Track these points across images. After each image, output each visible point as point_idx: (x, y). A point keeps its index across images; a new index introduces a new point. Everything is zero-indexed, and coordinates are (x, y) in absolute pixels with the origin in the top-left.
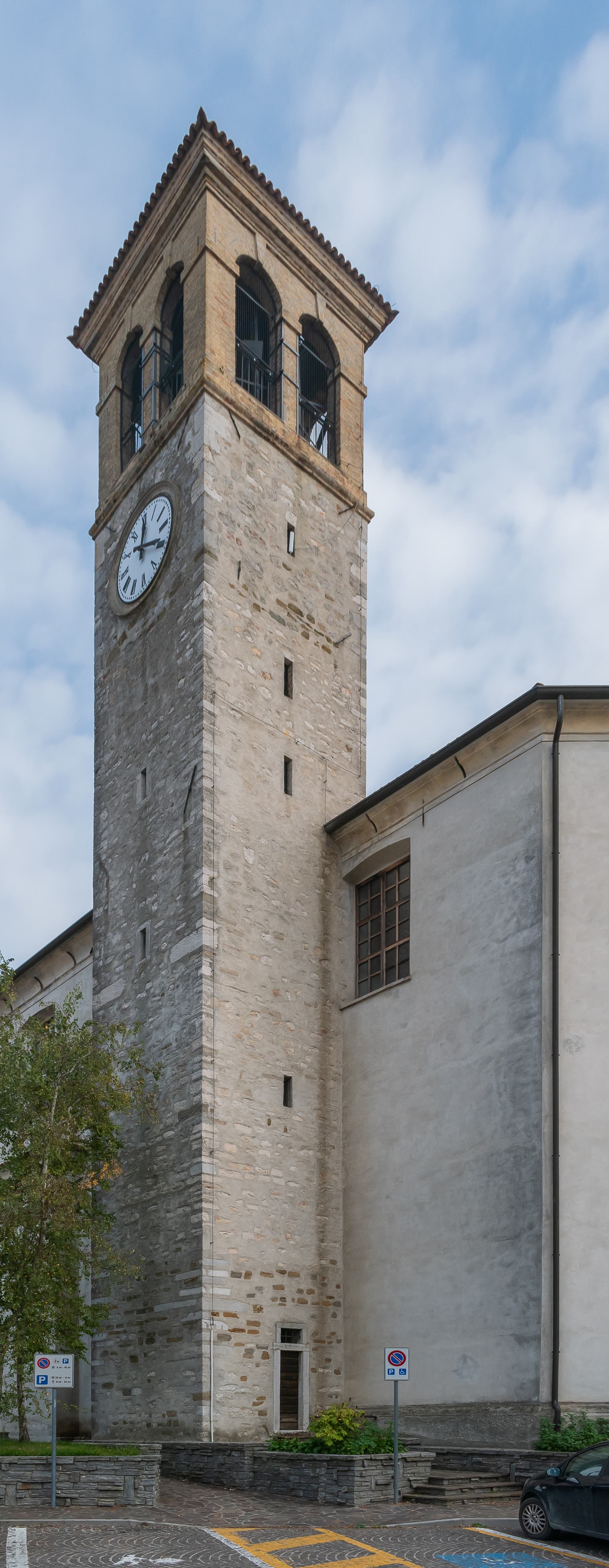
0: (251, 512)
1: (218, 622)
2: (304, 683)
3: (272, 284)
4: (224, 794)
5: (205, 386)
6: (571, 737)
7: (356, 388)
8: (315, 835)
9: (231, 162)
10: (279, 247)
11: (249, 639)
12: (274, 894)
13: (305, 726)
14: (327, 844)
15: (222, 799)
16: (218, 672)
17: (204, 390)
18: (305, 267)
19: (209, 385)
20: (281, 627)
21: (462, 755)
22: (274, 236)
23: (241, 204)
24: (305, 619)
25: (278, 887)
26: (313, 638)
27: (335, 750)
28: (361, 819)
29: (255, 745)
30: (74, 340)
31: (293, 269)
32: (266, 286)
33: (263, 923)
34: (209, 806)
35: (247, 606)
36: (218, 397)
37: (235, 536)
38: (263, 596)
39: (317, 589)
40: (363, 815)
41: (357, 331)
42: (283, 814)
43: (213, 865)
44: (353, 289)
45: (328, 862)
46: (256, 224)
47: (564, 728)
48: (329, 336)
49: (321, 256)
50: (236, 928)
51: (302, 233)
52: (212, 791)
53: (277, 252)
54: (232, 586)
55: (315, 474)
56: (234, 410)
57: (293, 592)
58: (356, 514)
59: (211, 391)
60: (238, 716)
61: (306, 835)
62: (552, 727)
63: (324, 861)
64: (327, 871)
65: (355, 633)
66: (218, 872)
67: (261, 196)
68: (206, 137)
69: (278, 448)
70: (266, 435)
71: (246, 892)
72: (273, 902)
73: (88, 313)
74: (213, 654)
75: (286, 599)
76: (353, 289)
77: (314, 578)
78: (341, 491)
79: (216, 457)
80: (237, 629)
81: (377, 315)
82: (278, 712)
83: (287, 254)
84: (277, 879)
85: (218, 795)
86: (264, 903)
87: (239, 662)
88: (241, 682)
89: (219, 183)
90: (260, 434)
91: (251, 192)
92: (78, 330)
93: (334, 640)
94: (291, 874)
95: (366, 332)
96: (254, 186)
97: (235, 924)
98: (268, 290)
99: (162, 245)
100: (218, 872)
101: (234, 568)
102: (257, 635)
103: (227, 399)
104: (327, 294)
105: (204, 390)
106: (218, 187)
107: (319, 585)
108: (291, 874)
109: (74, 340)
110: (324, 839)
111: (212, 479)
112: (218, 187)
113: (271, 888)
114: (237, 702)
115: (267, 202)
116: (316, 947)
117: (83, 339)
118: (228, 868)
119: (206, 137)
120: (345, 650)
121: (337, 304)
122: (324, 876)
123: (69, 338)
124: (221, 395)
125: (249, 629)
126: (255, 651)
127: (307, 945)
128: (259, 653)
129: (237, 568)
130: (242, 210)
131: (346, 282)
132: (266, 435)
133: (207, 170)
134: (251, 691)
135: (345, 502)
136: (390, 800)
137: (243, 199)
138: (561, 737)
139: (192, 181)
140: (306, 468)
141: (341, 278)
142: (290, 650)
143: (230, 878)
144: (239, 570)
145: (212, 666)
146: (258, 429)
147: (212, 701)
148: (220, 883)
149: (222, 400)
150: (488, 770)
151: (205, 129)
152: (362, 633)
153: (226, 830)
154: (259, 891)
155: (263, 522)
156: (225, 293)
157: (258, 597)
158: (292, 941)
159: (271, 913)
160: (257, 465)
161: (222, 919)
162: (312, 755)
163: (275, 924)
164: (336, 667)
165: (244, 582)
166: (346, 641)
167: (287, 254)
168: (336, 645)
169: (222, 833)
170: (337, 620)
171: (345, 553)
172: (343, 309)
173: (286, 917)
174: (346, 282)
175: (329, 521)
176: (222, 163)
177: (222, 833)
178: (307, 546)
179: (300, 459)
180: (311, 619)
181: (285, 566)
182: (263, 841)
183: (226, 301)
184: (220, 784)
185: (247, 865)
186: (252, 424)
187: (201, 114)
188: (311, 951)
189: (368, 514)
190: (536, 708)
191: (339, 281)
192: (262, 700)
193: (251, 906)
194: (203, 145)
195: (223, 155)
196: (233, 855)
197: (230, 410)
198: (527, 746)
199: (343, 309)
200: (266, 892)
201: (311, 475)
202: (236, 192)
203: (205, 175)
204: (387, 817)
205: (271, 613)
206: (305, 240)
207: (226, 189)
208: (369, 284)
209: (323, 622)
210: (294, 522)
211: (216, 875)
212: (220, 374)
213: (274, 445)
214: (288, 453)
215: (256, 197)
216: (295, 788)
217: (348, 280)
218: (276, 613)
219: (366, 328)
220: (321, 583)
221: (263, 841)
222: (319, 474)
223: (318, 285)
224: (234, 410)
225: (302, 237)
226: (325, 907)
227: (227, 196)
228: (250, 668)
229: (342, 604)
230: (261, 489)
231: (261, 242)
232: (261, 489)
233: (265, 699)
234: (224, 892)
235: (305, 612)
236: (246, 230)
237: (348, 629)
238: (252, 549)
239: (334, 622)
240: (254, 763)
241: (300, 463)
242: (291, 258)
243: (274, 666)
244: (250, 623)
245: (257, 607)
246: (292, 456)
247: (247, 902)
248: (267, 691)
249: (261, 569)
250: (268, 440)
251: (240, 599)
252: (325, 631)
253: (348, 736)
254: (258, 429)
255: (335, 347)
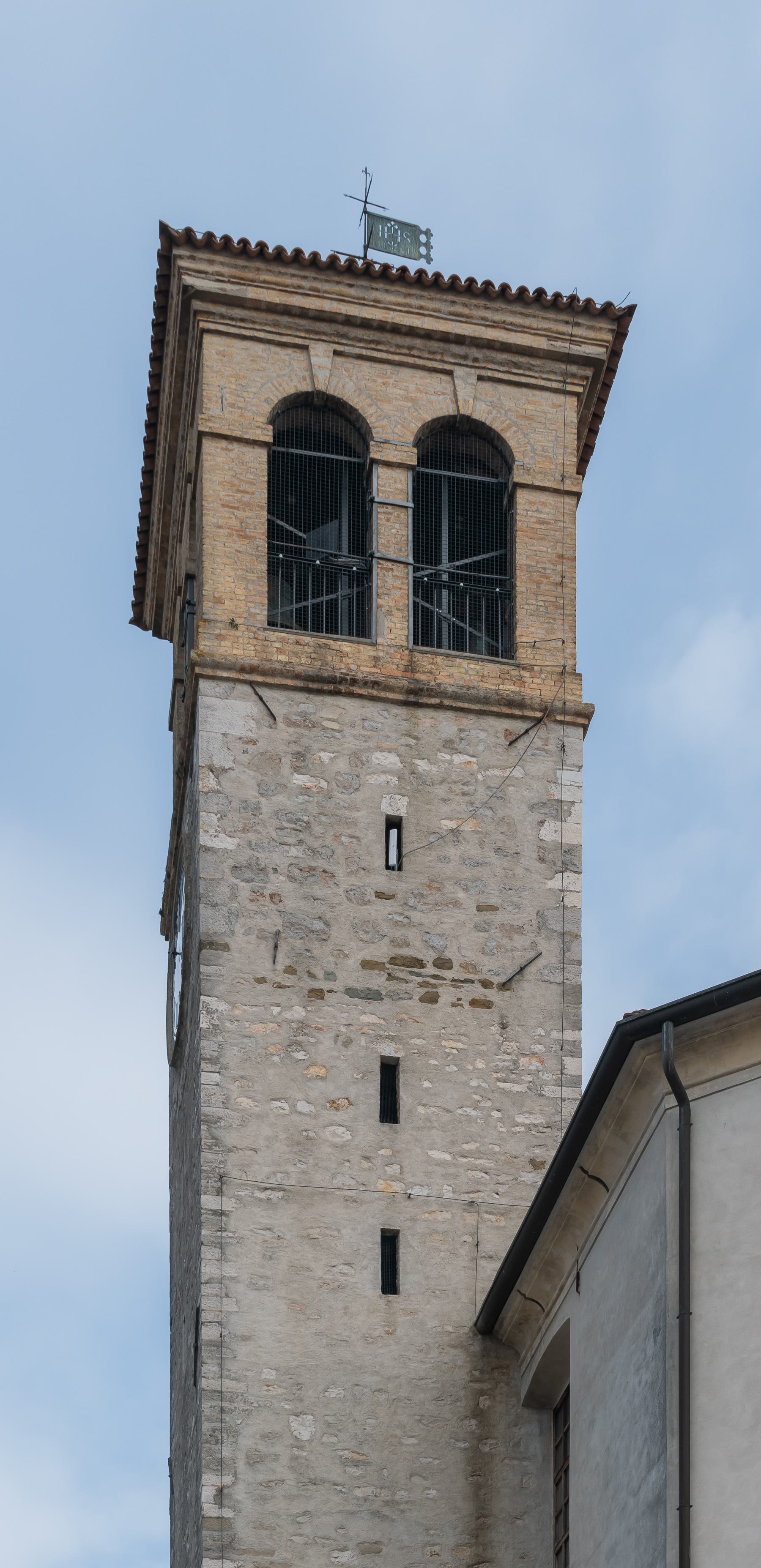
0: (301, 836)
1: (232, 1056)
2: (426, 1084)
3: (353, 410)
4: (245, 1338)
5: (197, 670)
6: (708, 1088)
7: (556, 491)
8: (455, 1347)
9: (235, 267)
10: (361, 340)
11: (300, 1055)
12: (357, 1478)
13: (430, 1161)
14: (485, 1353)
15: (242, 1350)
16: (230, 1138)
17: (198, 676)
18: (418, 342)
19: (204, 665)
20: (374, 1005)
21: (585, 1159)
22: (345, 329)
23: (271, 317)
24: (430, 970)
25: (367, 1463)
26: (447, 995)
27: (502, 1179)
28: (515, 1301)
29: (314, 1233)
30: (138, 621)
31: (397, 358)
32: (342, 416)
33: (333, 1535)
34: (216, 1369)
35: (295, 999)
36: (225, 674)
37: (267, 892)
38: (331, 968)
39: (456, 904)
40: (514, 1293)
41: (555, 385)
42: (379, 1331)
43: (221, 1465)
44: (527, 322)
45: (485, 1386)
46: (308, 331)
47: (684, 1078)
48: (490, 429)
49: (446, 308)
50: (274, 1558)
51: (398, 293)
52: (219, 1345)
53: (357, 351)
54: (261, 981)
55: (446, 702)
56: (260, 679)
57: (399, 934)
58: (552, 726)
59: (210, 672)
60: (275, 1196)
61: (434, 1353)
62: (664, 1086)
63: (477, 1386)
64: (484, 1402)
65: (550, 948)
66: (235, 1475)
67: (303, 283)
68: (181, 257)
69: (361, 696)
70: (331, 687)
71: (295, 1491)
72: (358, 1493)
73: (140, 576)
74: (221, 1112)
75: (382, 951)
76: (527, 322)
77: (449, 887)
78: (510, 703)
79: (223, 779)
80: (272, 1050)
81: (591, 334)
82: (366, 1158)
83: (378, 342)
84: (365, 1449)
85: (234, 1346)
86: (336, 1499)
87: (278, 1104)
88: (283, 1136)
89: (223, 310)
90: (319, 692)
91: (284, 289)
92: (138, 606)
93: (496, 980)
94: (398, 1432)
95: (574, 376)
96: (289, 277)
97: (271, 1553)
98: (351, 422)
99: (183, 437)
100: (235, 1475)
101: (265, 949)
102: (318, 1042)
103: (242, 670)
104: (476, 360)
105: (198, 676)
106: (223, 316)
107: (461, 895)
108: (398, 1432)
109: (138, 621)
110: (476, 1347)
111: (214, 818)
112: (223, 316)
113: (352, 1470)
114: (275, 1173)
115: (318, 285)
116: (458, 1546)
117: (148, 617)
118: (255, 1460)
119: (181, 257)
120: (527, 988)
121: (501, 364)
122: (478, 1413)
123: (132, 622)
124: (229, 669)
125: (300, 1038)
126: (313, 1071)
127: (437, 1548)
128: (322, 1072)
129: (271, 944)
130: (276, 324)
131: (510, 319)
132: (331, 687)
133: (197, 305)
134: (303, 1144)
135: (523, 718)
136: (535, 1258)
137: (272, 309)
138: (691, 1094)
139: (184, 331)
140: (425, 700)
141: (498, 317)
142: (392, 1039)
143: (261, 1477)
144: (276, 947)
145: (218, 1133)
146: (315, 686)
147: (219, 1192)
148: (240, 1493)
149: (233, 675)
150: (625, 1176)
151: (178, 246)
152: (569, 939)
153: (251, 1399)
154: (323, 1481)
155: (329, 841)
156: (244, 487)
157: (320, 974)
158: (402, 1548)
159: (352, 1513)
160: (315, 746)
161: (244, 1552)
162: (446, 1205)
163: (362, 1529)
164: (504, 1026)
165: (288, 962)
166: (528, 969)
167: (378, 342)
168: (505, 986)
169: (242, 1406)
170: (505, 941)
171: (524, 808)
172: (517, 365)
173: (386, 1511)
174: (510, 319)
175: (487, 768)
176: (218, 277)
177: (242, 1406)
178: (432, 838)
179: (410, 692)
180: (443, 963)
181: (380, 895)
182: (333, 1393)
183: (246, 498)
184: (238, 1325)
185: (298, 1444)
186: (299, 683)
187: (164, 229)
188: (446, 1557)
189: (578, 714)
190: (641, 1056)
191: (495, 325)
192: (329, 1150)
193: (306, 1513)
194: (182, 271)
195: (221, 265)
196: (265, 1437)
197: (251, 684)
198: (654, 1123)
199: (517, 365)
200: (340, 1480)
201: (439, 707)
202: (257, 306)
203: (196, 312)
204: (547, 1287)
205: (351, 992)
206: (408, 300)
207: (237, 312)
208: (557, 296)
209: (472, 956)
210: (399, 807)
211: (228, 1480)
212: (233, 632)
213: (351, 695)
214: (383, 694)
215: (296, 291)
216: (406, 1278)
217: (514, 313)
218: (359, 986)
219: (573, 369)
220: (466, 890)
221: (333, 1393)
222: (455, 697)
223: (454, 355)
224: (260, 679)
225: (400, 300)
226: (479, 1469)
227: (242, 320)
228: (302, 1106)
229: (518, 907)
230: (324, 784)
231: (321, 354)
232: (324, 784)
233: (335, 1146)
234: (248, 1506)
235: (429, 956)
236: (290, 351)
237: (534, 944)
238: (306, 898)
239: (499, 946)
240: (313, 1265)
241: (412, 698)
242: (389, 343)
243: (356, 1081)
244: (303, 1026)
245: (317, 994)
246: (391, 696)
247: (297, 1507)
248: (340, 1130)
249: (327, 924)
250: (337, 693)
251: (281, 996)
252: (476, 972)
253: (535, 1142)
254: (315, 686)
255: (503, 441)
